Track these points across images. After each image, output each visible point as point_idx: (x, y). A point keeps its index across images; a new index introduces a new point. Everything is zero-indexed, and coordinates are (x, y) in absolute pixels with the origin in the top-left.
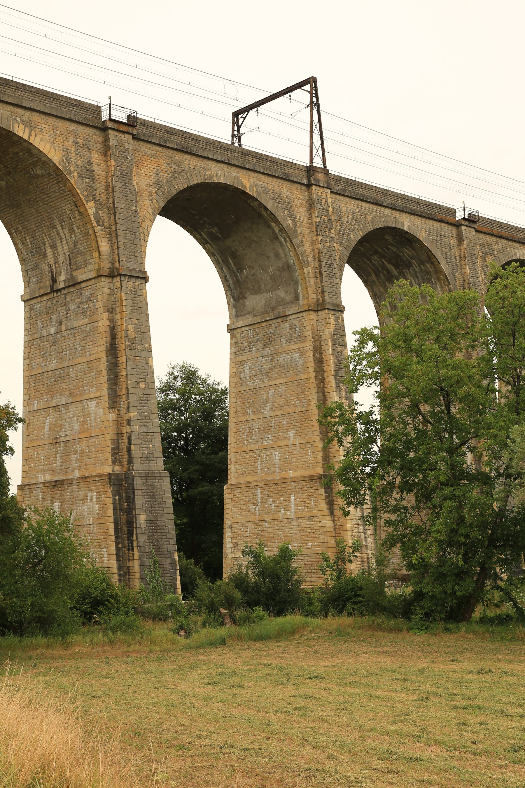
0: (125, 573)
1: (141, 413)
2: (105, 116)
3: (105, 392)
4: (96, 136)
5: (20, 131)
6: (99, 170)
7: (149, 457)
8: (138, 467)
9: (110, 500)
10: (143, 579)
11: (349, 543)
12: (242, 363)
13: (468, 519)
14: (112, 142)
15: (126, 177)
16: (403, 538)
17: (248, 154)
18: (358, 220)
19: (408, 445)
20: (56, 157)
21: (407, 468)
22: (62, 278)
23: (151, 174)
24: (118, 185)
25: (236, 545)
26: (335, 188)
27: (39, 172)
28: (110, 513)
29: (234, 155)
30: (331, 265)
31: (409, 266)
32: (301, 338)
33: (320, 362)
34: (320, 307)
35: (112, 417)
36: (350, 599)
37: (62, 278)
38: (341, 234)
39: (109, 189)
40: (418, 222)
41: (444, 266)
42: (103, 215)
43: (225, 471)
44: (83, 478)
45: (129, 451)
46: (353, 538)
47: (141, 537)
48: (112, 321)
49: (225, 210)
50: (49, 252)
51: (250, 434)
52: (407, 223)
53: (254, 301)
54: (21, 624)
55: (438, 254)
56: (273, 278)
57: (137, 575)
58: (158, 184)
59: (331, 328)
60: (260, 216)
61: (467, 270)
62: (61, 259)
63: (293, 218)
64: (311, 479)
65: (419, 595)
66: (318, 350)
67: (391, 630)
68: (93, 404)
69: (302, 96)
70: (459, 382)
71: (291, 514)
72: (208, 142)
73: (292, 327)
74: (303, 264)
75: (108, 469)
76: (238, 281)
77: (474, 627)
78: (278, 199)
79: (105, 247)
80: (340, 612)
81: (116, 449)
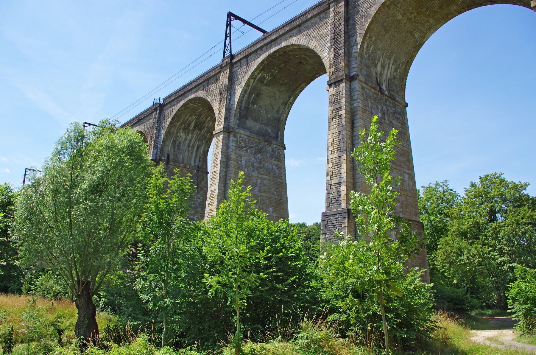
69: (235, 23)
76: (248, 108)
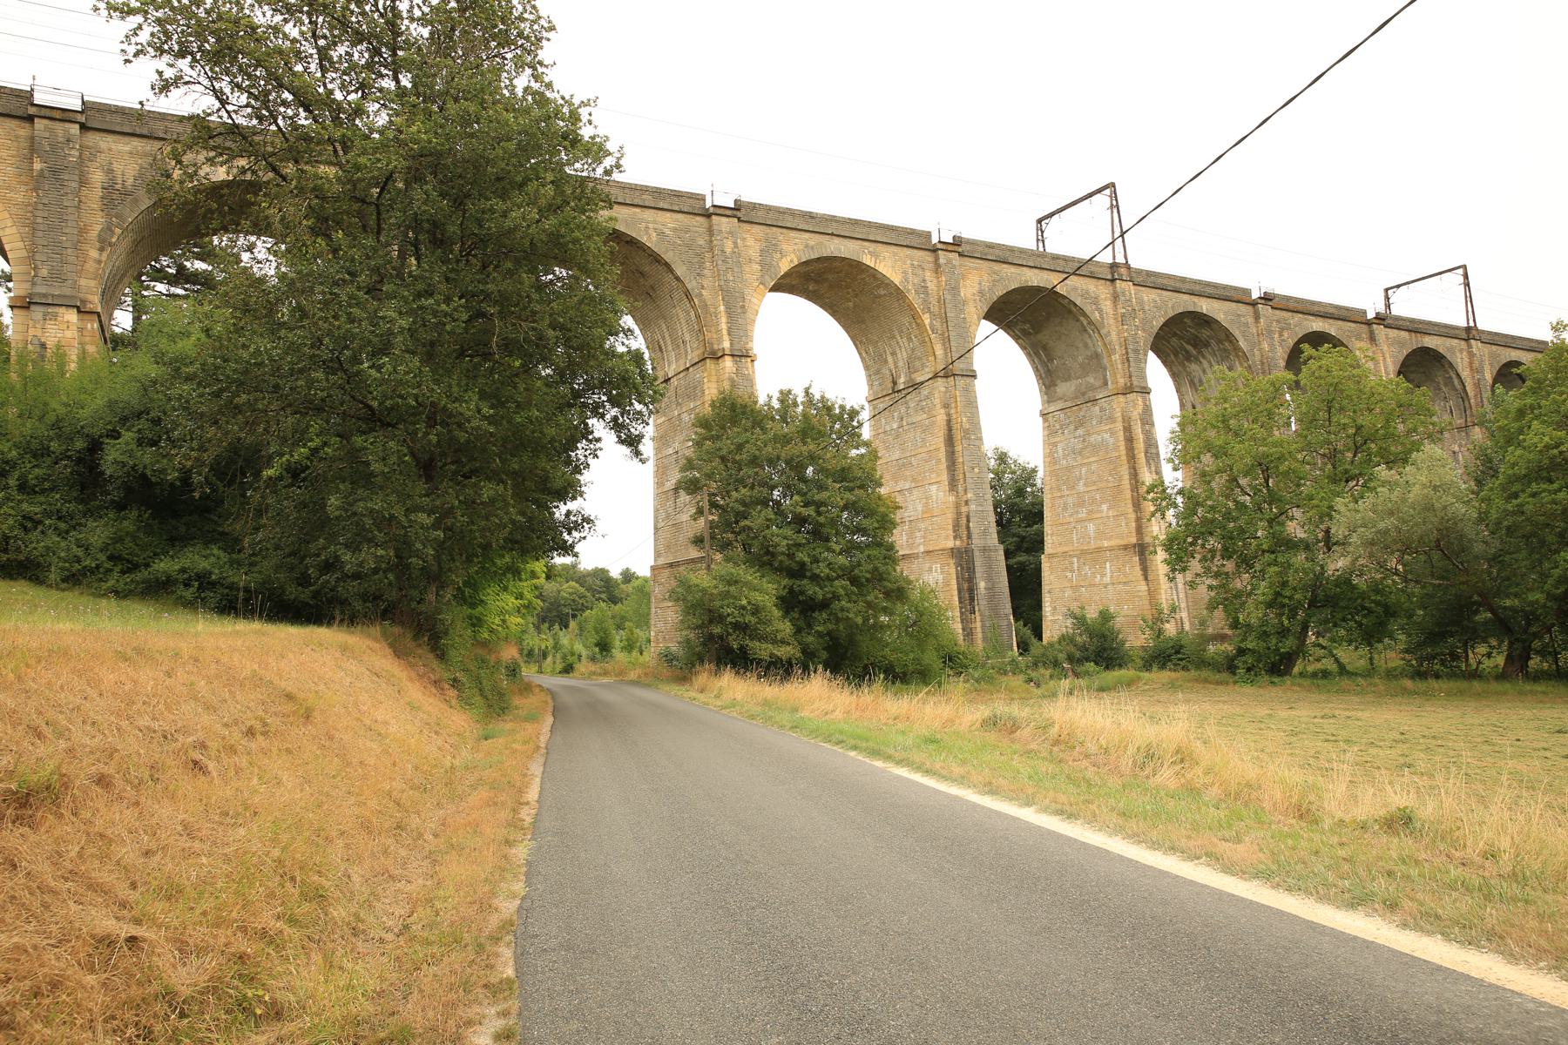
0: (969, 633)
1: (977, 495)
2: (935, 240)
3: (945, 477)
4: (928, 257)
5: (868, 260)
6: (931, 286)
7: (985, 533)
8: (977, 541)
9: (953, 571)
10: (985, 639)
11: (1165, 606)
12: (1055, 444)
13: (1292, 582)
14: (942, 261)
15: (955, 290)
16: (1228, 600)
17: (1056, 257)
18: (1159, 308)
19: (1228, 516)
20: (896, 279)
21: (1228, 537)
22: (902, 380)
23: (977, 285)
24: (948, 297)
25: (1055, 609)
26: (1139, 280)
27: (883, 292)
28: (954, 582)
29: (1039, 260)
30: (1136, 351)
31: (1207, 345)
32: (1112, 419)
33: (1130, 440)
34: (1128, 390)
35: (952, 499)
36: (1168, 656)
37: (902, 380)
38: (1144, 321)
39: (942, 302)
40: (1216, 304)
41: (1242, 344)
42: (937, 324)
43: (1042, 542)
44: (928, 552)
45: (968, 527)
46: (1178, 600)
47: (982, 603)
48: (948, 415)
49: (1037, 313)
50: (890, 359)
51: (1065, 508)
52: (1204, 306)
53: (1064, 388)
54: (905, 674)
55: (1237, 333)
56: (1082, 366)
57: (979, 635)
58: (981, 292)
59: (1140, 409)
60: (1070, 311)
61: (1265, 346)
62: (901, 364)
63: (1100, 311)
64: (1126, 547)
65: (1241, 652)
66: (1128, 429)
67: (1218, 683)
68: (934, 488)
69: (1103, 200)
70: (1281, 458)
71: (1107, 579)
72: (1022, 251)
73: (1102, 410)
74: (1110, 352)
75: (950, 544)
77: (1299, 680)
78: (1085, 294)
79: (939, 352)
80: (1163, 667)
81: (956, 527)
